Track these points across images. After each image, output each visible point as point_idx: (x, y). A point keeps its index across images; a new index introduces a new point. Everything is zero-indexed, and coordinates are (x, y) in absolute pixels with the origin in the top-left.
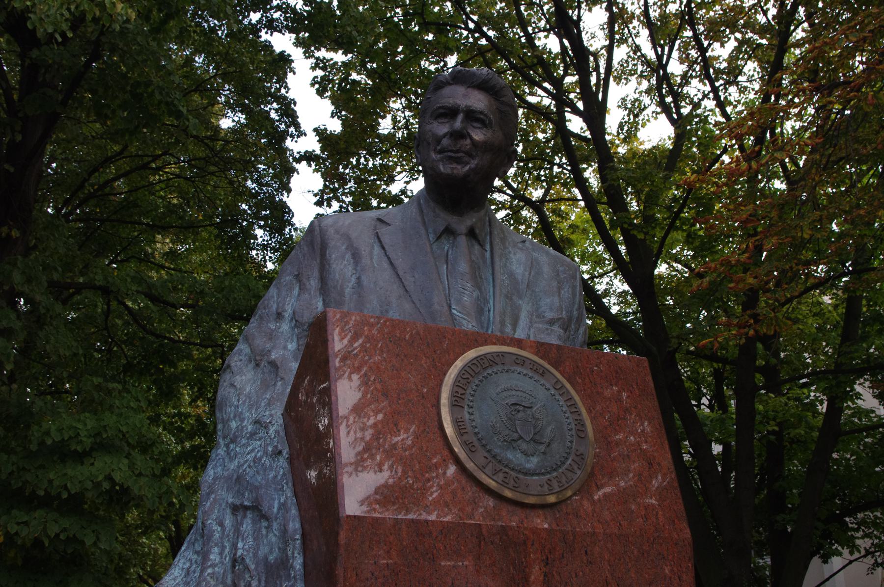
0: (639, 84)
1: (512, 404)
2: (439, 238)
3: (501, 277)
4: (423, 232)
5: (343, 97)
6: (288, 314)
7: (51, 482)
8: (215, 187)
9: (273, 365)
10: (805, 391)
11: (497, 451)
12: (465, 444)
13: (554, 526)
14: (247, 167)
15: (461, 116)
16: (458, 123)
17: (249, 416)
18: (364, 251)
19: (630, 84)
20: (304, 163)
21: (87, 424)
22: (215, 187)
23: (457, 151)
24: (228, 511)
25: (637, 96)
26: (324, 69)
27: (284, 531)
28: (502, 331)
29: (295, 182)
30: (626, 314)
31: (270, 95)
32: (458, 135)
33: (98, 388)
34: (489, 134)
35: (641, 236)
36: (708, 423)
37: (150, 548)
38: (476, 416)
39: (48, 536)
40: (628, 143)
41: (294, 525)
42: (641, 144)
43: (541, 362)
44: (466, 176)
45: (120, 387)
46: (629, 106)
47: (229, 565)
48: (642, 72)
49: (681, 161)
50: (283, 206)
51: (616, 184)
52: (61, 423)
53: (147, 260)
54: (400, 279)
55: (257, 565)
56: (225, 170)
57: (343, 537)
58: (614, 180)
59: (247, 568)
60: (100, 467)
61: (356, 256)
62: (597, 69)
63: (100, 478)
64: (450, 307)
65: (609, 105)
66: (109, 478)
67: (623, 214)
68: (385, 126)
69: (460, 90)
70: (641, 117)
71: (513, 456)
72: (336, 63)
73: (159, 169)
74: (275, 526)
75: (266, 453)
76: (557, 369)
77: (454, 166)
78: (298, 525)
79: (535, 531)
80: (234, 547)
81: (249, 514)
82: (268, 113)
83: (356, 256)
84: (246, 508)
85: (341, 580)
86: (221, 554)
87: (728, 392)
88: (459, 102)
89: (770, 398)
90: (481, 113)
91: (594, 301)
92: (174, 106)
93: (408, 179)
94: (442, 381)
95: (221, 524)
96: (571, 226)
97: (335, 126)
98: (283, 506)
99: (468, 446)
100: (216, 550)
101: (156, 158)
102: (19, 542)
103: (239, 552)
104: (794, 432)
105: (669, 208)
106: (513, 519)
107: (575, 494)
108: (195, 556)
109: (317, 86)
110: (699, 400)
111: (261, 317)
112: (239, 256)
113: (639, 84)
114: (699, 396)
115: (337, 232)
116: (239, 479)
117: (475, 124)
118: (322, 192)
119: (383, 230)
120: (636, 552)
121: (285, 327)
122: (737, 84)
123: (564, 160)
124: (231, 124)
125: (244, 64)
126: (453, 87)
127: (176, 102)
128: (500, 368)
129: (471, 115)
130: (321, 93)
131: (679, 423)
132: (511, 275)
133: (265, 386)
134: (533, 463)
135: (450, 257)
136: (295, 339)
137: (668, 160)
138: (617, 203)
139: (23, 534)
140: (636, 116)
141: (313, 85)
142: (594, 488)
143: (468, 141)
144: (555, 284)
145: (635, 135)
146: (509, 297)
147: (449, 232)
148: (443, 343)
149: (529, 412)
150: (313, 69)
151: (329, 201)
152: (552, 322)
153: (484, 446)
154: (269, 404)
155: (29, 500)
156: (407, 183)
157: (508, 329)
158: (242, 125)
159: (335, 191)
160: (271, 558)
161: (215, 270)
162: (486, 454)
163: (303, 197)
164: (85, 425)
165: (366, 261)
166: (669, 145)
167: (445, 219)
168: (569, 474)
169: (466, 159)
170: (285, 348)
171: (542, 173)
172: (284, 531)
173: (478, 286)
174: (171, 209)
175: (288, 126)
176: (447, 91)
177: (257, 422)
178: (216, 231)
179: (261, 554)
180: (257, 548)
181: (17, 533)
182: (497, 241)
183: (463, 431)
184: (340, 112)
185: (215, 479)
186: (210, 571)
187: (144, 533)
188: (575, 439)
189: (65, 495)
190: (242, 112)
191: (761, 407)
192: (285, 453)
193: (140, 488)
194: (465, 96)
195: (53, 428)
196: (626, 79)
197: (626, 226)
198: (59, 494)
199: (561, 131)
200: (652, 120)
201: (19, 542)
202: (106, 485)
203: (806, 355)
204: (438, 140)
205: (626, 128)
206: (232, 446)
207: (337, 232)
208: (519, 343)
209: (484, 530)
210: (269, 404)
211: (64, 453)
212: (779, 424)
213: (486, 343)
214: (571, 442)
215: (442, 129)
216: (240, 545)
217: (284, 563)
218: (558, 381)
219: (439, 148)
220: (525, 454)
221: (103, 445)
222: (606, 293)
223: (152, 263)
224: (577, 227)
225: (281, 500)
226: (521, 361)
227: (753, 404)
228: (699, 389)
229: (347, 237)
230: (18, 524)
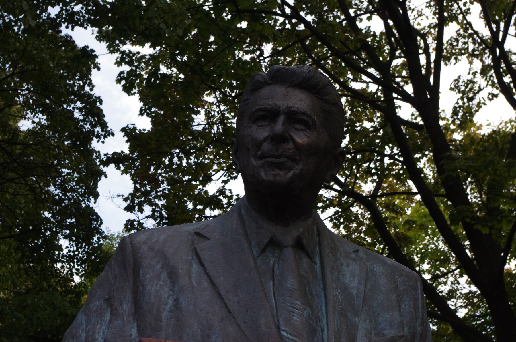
2: (263, 251)
5: (153, 93)
14: (50, 173)
15: (281, 119)
16: (279, 126)
20: (112, 166)
23: (279, 157)
25: (470, 77)
26: (130, 63)
31: (73, 93)
32: (279, 139)
35: (485, 231)
48: (474, 50)
54: (222, 299)
61: (173, 276)
64: (278, 328)
68: (199, 120)
69: (280, 90)
77: (277, 172)
82: (71, 113)
83: (173, 276)
88: (279, 103)
90: (304, 113)
93: (225, 178)
112: (42, 269)
117: (298, 126)
118: (133, 196)
119: (201, 245)
123: (395, 151)
129: (293, 117)
132: (345, 290)
135: (277, 272)
140: (470, 99)
141: (118, 81)
144: (394, 297)
145: (471, 121)
147: (274, 244)
156: (226, 182)
158: (43, 127)
159: (146, 194)
161: (15, 286)
163: (112, 201)
173: (308, 303)
175: (94, 126)
176: (265, 91)
184: (150, 109)
197: (468, 220)
204: (259, 145)
205: (460, 114)
207: (151, 249)
219: (259, 153)
222: (452, 294)
224: (414, 222)
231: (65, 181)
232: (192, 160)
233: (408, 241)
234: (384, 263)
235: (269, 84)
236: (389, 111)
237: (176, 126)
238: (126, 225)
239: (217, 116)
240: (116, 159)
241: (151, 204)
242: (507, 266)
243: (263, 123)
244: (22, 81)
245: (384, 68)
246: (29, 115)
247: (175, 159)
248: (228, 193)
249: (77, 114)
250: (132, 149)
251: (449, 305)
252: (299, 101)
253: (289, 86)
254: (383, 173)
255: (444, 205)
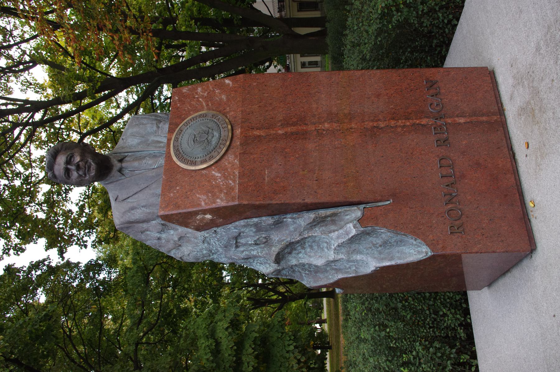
0: (12, 81)
2: (123, 174)
3: (139, 148)
4: (121, 181)
5: (26, 237)
6: (158, 235)
7: (229, 355)
8: (78, 300)
9: (180, 239)
10: (175, 6)
11: (212, 148)
12: (210, 159)
13: (240, 126)
14: (67, 286)
15: (69, 166)
16: (73, 168)
17: (201, 246)
18: (131, 205)
19: (12, 87)
20: (64, 255)
21: (203, 343)
22: (78, 300)
23: (85, 168)
24: (238, 249)
25: (19, 83)
26: (9, 249)
27: (245, 226)
28: (163, 147)
29: (74, 260)
30: (137, 91)
31: (27, 275)
32: (78, 167)
33: (185, 341)
34: (76, 154)
35: (99, 84)
36: (191, 54)
37: (258, 316)
38: (199, 156)
39: (253, 352)
40: (46, 88)
41: (242, 222)
42: (46, 81)
43: (176, 131)
44: (96, 163)
45: (184, 331)
46: (25, 87)
47: (258, 246)
48: (5, 80)
49: (56, 61)
50: (87, 266)
51: (72, 96)
52: (203, 354)
53: (118, 332)
55: (257, 235)
56: (70, 296)
57: (245, 202)
58: (70, 97)
59: (258, 239)
60: (222, 334)
61: (133, 208)
63: (227, 333)
65: (24, 99)
66: (227, 329)
67: (88, 93)
68: (41, 215)
69: (56, 167)
70: (31, 81)
71: (214, 141)
72: (6, 243)
73: (70, 329)
74: (242, 230)
75: (216, 237)
76: (179, 125)
77: (92, 169)
78: (242, 221)
79: (241, 133)
80: (250, 245)
81: (239, 241)
82: (38, 276)
83: (133, 208)
84: (236, 242)
85: (260, 202)
86: (254, 250)
87: (175, 43)
88: (62, 168)
89: (179, 23)
90: (67, 158)
91: (131, 108)
92: (42, 318)
93: (70, 203)
94: (186, 169)
95: (243, 252)
96: (93, 119)
97: (42, 241)
98: (235, 228)
99: (211, 158)
100: (252, 252)
101: (65, 332)
102: (256, 365)
103: (253, 242)
104: (195, 13)
105: (85, 70)
106: (237, 142)
107: (227, 117)
108: (255, 261)
109: (19, 253)
110: (180, 57)
111: (160, 246)
112: (114, 285)
113: (12, 81)
114: (178, 57)
115: (122, 217)
116: (226, 247)
117: (72, 160)
118: (80, 245)
119: (120, 198)
121: (164, 236)
122: (11, 31)
123: (58, 122)
124: (44, 295)
125: (11, 290)
126: (55, 170)
127: (40, 317)
128: (179, 147)
129: (68, 162)
130: (23, 250)
131: (192, 68)
132: (139, 144)
133: (189, 241)
134: (216, 134)
135: (132, 169)
136: (169, 231)
137: (55, 68)
138: (82, 96)
139: (252, 363)
140: (31, 84)
141: (19, 255)
142: (225, 111)
144: (141, 126)
145: (42, 85)
146: (148, 145)
147: (120, 170)
148: (171, 169)
149: (196, 136)
150: (9, 255)
151: (84, 242)
152: (158, 127)
154: (196, 238)
155: (239, 362)
156: (72, 203)
157: (162, 145)
158: (44, 290)
159: (78, 240)
160: (254, 230)
161: (122, 297)
163: (81, 255)
164: (203, 343)
165: (135, 204)
166: (46, 67)
167: (115, 172)
168: (220, 120)
169: (88, 164)
170: (173, 235)
171: (65, 133)
172: (245, 226)
173: (144, 157)
174: (91, 322)
175: (45, 265)
176: (57, 173)
177: (203, 242)
178: (102, 298)
179: (253, 234)
180: (251, 236)
181: (253, 367)
182: (123, 150)
184: (34, 239)
185: (226, 257)
186: (260, 254)
187: (251, 319)
188: (206, 118)
189: (235, 348)
190: (37, 289)
191: (184, 27)
192: (215, 229)
193: (230, 315)
194: (59, 165)
195: (205, 357)
196: (9, 88)
197: (94, 91)
198: (235, 350)
199: (42, 123)
200: (33, 76)
201: (256, 365)
202: (230, 330)
203: (157, 3)
204: (80, 176)
205: (38, 90)
206: (213, 252)
207: (122, 217)
208: (169, 140)
209: (242, 152)
210: (196, 238)
211: (216, 351)
212: (192, 20)
213: (169, 153)
215: (75, 175)
216: (250, 243)
217: (256, 225)
218: (184, 125)
221: (212, 334)
222: (127, 101)
223: (119, 329)
224: (93, 116)
225: (233, 228)
226: (177, 139)
227: (182, 32)
228: (174, 56)
229: (124, 213)
230: (248, 366)
231: (71, 277)
232: (61, 219)
233: (101, 120)
234: (128, 129)
236: (36, 125)
237: (44, 226)
238: (94, 248)
239: (37, 207)
240: (61, 253)
241: (83, 237)
242: (114, 75)
244: (20, 300)
245: (15, 125)
246: (38, 296)
247: (61, 226)
248: (78, 201)
249: (39, 272)
250: (57, 246)
252: (61, 160)
254: (69, 129)
255: (86, 101)
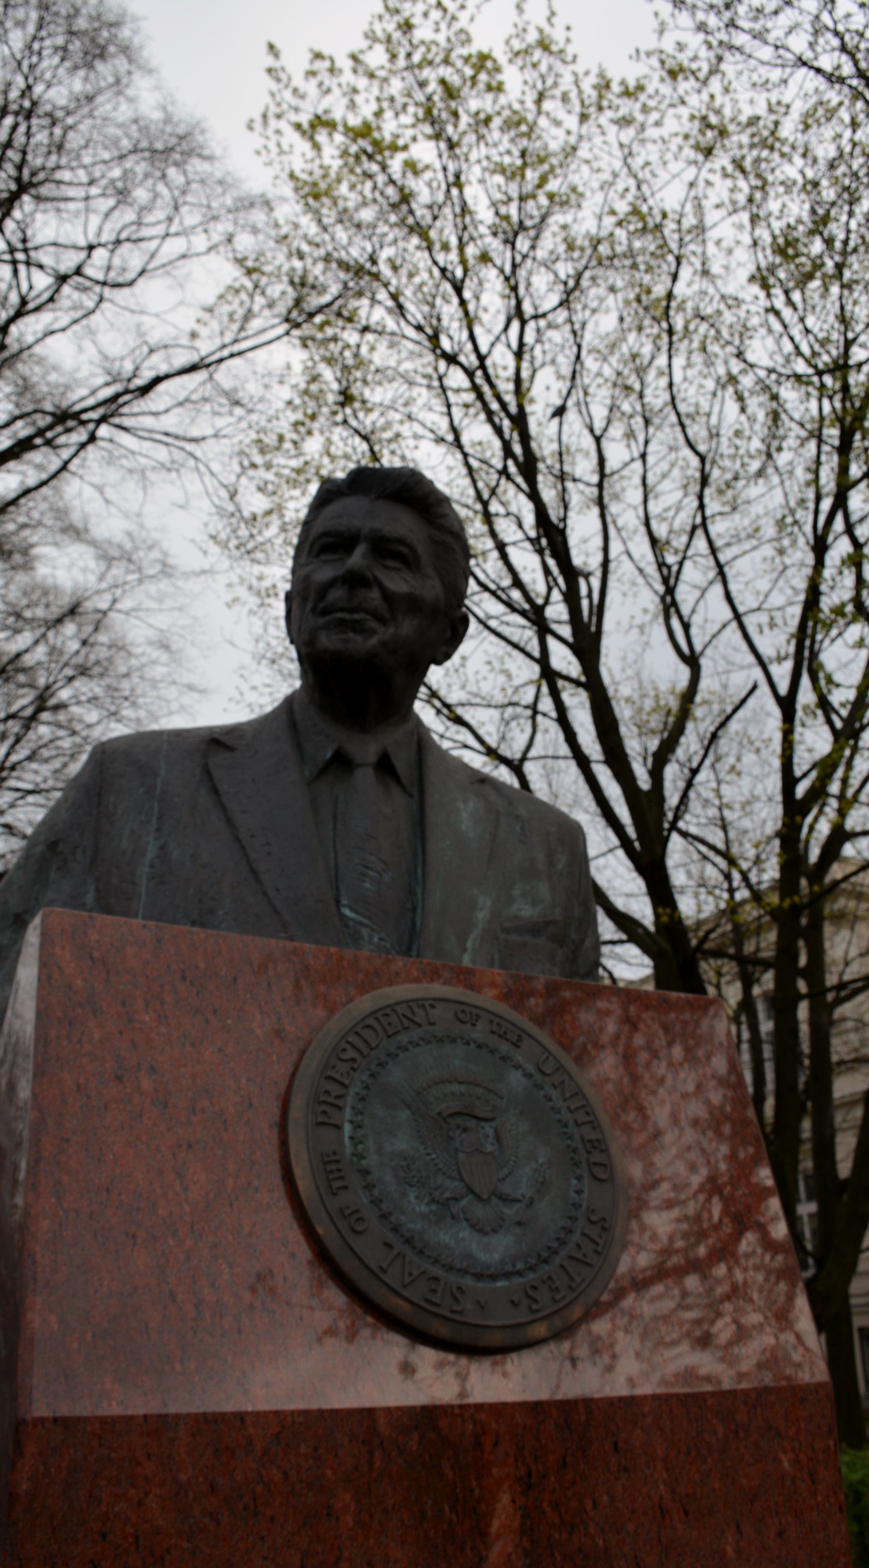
1: (452, 1115)
16: (358, 558)
23: (352, 611)
54: (243, 848)
62: (590, 595)
64: (338, 902)
117: (391, 563)
120: (721, 1431)
143: (375, 595)
153: (384, 1216)
162: (391, 1237)
167: (325, 741)
169: (373, 624)
183: (336, 1184)
214: (579, 1192)
219: (321, 606)
220: (478, 1228)
235: (347, 495)
243: (331, 557)
251: (447, 751)
253: (378, 498)
